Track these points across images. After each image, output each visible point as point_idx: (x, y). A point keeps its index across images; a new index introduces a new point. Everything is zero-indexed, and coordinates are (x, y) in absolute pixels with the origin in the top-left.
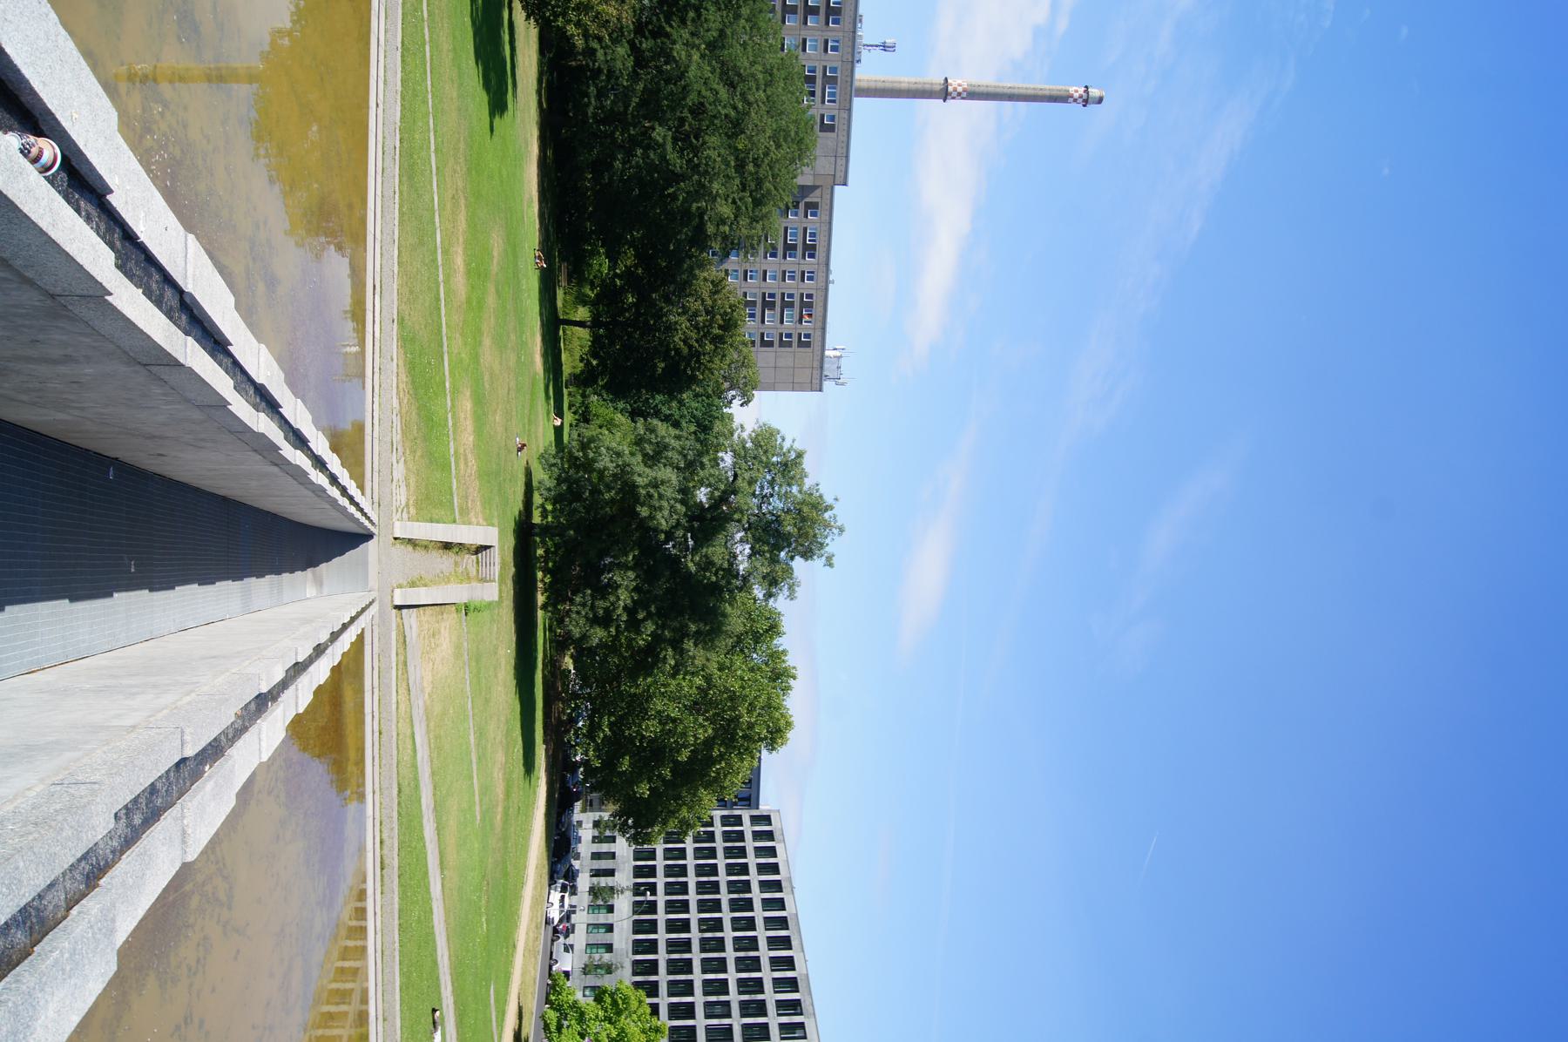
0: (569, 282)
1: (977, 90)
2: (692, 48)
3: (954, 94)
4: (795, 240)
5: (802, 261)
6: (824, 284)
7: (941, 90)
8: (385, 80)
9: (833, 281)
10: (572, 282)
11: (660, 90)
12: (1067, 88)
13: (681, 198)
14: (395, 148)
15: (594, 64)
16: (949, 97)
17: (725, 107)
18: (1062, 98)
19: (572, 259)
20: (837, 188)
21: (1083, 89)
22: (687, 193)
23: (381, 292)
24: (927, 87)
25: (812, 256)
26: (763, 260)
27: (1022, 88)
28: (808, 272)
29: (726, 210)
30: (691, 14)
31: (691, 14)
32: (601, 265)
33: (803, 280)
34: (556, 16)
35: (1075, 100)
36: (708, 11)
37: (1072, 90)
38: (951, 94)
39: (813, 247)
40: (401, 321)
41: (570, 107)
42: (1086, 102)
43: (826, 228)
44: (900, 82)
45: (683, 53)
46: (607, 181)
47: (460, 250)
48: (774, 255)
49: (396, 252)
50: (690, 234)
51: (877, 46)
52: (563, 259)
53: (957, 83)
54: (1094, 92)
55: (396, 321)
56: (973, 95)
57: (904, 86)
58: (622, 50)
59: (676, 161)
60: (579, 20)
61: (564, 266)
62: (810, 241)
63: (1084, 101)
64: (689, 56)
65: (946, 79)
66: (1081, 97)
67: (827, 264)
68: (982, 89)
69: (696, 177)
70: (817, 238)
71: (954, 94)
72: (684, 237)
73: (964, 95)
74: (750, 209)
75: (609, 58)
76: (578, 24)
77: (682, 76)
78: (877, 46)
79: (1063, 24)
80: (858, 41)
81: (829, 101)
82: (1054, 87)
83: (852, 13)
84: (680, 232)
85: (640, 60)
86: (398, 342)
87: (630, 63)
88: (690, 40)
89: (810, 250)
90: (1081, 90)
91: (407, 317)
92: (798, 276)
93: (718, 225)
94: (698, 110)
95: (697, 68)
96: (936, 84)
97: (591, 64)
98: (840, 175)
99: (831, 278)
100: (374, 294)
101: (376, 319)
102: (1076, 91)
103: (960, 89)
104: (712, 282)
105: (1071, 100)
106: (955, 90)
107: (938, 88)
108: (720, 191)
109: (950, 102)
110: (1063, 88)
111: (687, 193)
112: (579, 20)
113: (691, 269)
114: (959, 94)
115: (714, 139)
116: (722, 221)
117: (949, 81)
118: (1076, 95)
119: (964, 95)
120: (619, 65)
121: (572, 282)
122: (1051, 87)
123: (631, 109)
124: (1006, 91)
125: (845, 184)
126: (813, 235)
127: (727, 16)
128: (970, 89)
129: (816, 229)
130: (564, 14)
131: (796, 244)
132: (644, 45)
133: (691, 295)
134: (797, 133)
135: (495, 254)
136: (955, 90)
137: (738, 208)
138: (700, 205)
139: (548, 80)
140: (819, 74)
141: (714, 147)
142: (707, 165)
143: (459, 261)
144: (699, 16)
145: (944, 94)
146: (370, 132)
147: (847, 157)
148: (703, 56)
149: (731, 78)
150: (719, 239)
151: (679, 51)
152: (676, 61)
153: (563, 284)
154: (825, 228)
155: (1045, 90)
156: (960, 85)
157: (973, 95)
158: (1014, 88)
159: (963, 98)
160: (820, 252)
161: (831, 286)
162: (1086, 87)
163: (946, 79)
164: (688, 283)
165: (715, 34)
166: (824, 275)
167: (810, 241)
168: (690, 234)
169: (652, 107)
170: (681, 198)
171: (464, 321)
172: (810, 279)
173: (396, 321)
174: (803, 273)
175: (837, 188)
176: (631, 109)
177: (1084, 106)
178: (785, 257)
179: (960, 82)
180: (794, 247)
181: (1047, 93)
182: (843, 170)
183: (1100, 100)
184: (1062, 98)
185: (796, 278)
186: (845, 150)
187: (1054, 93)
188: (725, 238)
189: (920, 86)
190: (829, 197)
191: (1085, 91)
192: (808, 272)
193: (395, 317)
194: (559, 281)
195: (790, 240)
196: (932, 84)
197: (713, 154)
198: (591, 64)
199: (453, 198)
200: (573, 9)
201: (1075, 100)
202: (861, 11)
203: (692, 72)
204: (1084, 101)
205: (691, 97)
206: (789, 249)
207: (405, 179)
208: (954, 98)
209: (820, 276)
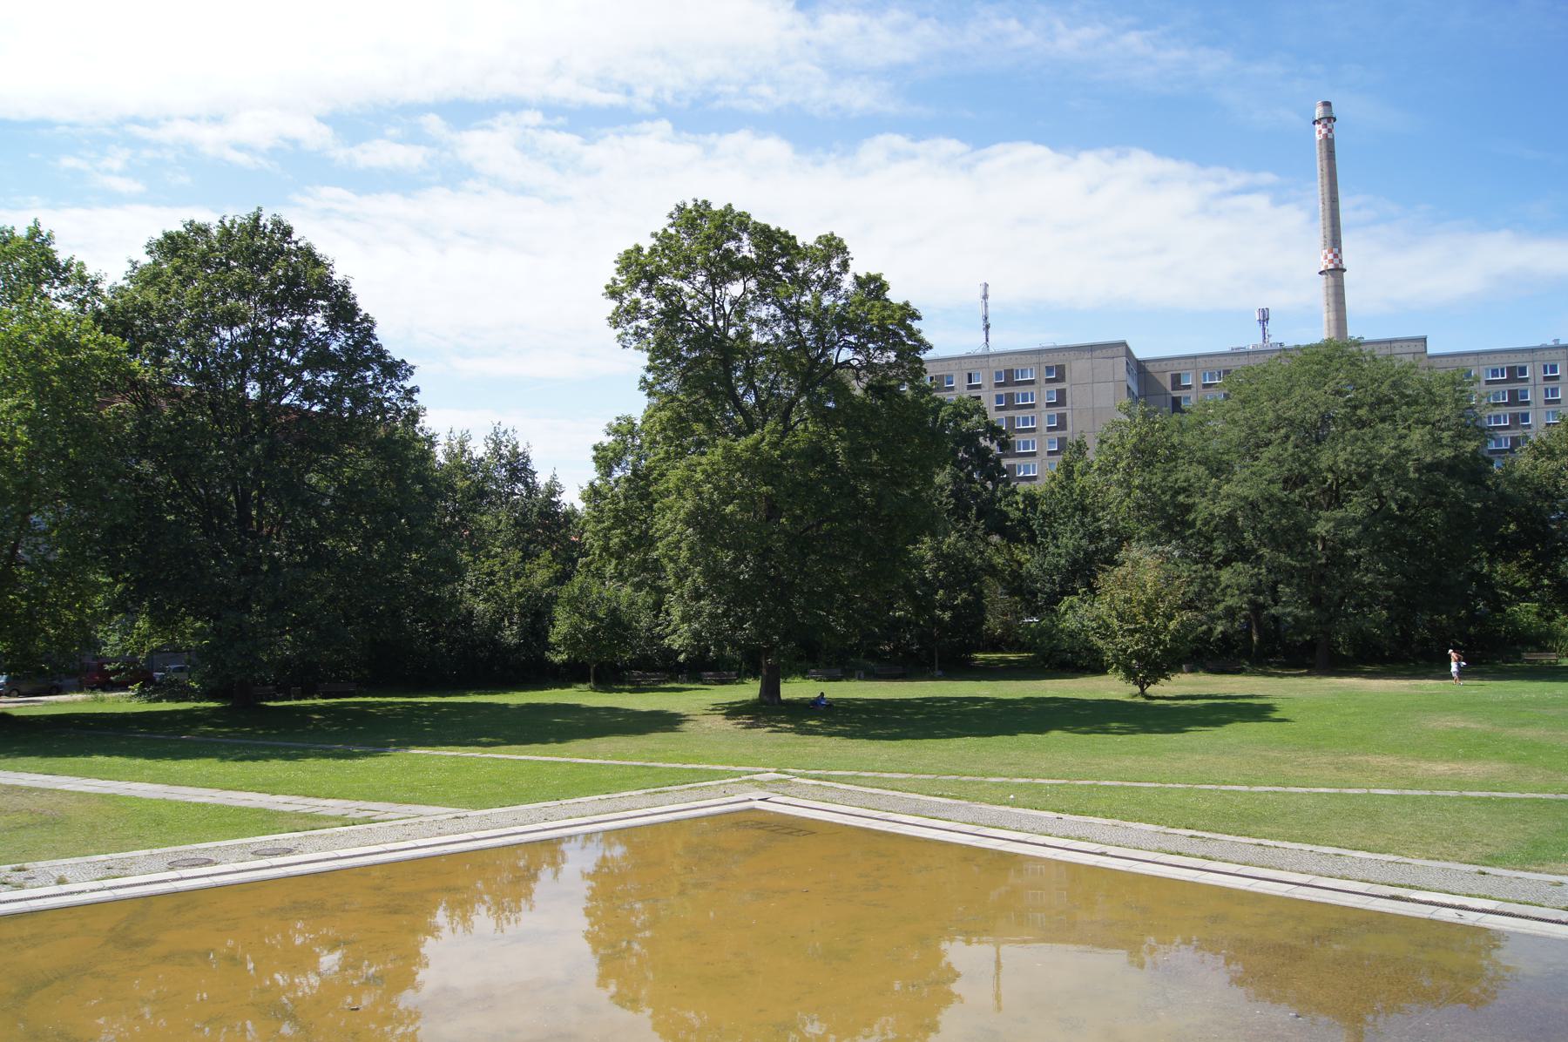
0: (1551, 650)
1: (1329, 238)
2: (1219, 494)
3: (1336, 261)
4: (1504, 392)
5: (1531, 382)
6: (1560, 351)
7: (1333, 276)
8: (1203, 857)
9: (1555, 340)
10: (1551, 647)
11: (1270, 529)
12: (1317, 143)
13: (1404, 494)
14: (1192, 837)
15: (1244, 609)
16: (1340, 266)
17: (1286, 450)
18: (1329, 145)
19: (1518, 647)
20: (1430, 351)
21: (1317, 126)
22: (1397, 485)
23: (1411, 887)
24: (1331, 291)
25: (1523, 370)
26: (1533, 429)
27: (1323, 190)
28: (1545, 372)
29: (1417, 437)
30: (1181, 498)
31: (1181, 498)
32: (1528, 612)
33: (1557, 378)
34: (1159, 642)
35: (1330, 131)
36: (1176, 480)
37: (1318, 137)
38: (1336, 265)
39: (1511, 370)
40: (1493, 860)
41: (1300, 639)
42: (1330, 119)
43: (1485, 358)
44: (1328, 321)
45: (1223, 503)
46: (1391, 592)
47: (1424, 765)
48: (1525, 417)
49: (1359, 854)
50: (1458, 484)
51: (1264, 329)
52: (1519, 658)
53: (1323, 261)
54: (1319, 112)
55: (1483, 869)
56: (1335, 242)
57: (1332, 316)
58: (1225, 575)
59: (1356, 508)
60: (1164, 615)
61: (1526, 656)
62: (1503, 376)
63: (1329, 122)
64: (1228, 497)
65: (1320, 273)
66: (1325, 126)
67: (1533, 350)
68: (1328, 234)
69: (1376, 477)
70: (1498, 367)
71: (1336, 261)
72: (1461, 490)
73: (1336, 250)
74: (1419, 408)
75: (1237, 592)
76: (1170, 617)
77: (1253, 505)
78: (1264, 329)
79: (1267, 177)
80: (1259, 348)
81: (1032, 400)
82: (1318, 157)
83: (1228, 358)
84: (1455, 495)
85: (1243, 553)
86: (1527, 870)
87: (1239, 566)
88: (1209, 497)
89: (1515, 373)
90: (1318, 127)
91: (1489, 850)
92: (1551, 385)
93: (1442, 446)
94: (1290, 482)
95: (1242, 486)
96: (1327, 283)
97: (1244, 613)
98: (1413, 347)
99: (1550, 343)
100: (1408, 900)
101: (1457, 903)
102: (1320, 132)
103: (1330, 256)
104: (1536, 458)
105: (1330, 136)
106: (1331, 261)
107: (1331, 280)
108: (1392, 445)
109: (1345, 264)
110: (1317, 146)
111: (1397, 485)
112: (1164, 615)
113: (1512, 483)
114: (1336, 256)
115: (1323, 458)
116: (1437, 442)
117: (1323, 269)
118: (1324, 131)
119: (1336, 250)
120: (1244, 580)
121: (1551, 647)
122: (1318, 159)
123: (1293, 563)
124: (1327, 207)
125: (1424, 340)
126: (1495, 373)
127: (1183, 458)
128: (1328, 246)
129: (1487, 369)
130: (1156, 632)
131: (1509, 391)
132: (1220, 551)
133: (1556, 485)
134: (1319, 363)
135: (1462, 725)
136: (1331, 261)
137: (1418, 422)
138: (1412, 469)
139: (1275, 668)
140: (1003, 391)
141: (1334, 457)
142: (1358, 464)
143: (1441, 768)
144: (1184, 490)
145: (1336, 272)
146: (1131, 870)
147: (1391, 341)
148: (1228, 481)
149: (1253, 446)
150: (1461, 443)
151: (1221, 509)
152: (1235, 510)
153: (1552, 657)
154: (1485, 359)
155: (1322, 165)
156: (1326, 258)
157: (1335, 242)
158: (1323, 199)
159: (1340, 251)
160: (1515, 361)
161: (1561, 343)
162: (1314, 123)
163: (1320, 273)
164: (1539, 492)
165: (1202, 468)
166: (1547, 352)
167: (1503, 376)
168: (1458, 484)
169: (1294, 538)
170: (1404, 494)
171: (1545, 767)
172: (1554, 369)
173: (1483, 869)
174: (1546, 379)
175: (1430, 351)
176: (1293, 563)
177: (1335, 120)
178: (1527, 403)
179: (1322, 258)
180: (1513, 394)
181: (1325, 162)
182: (1406, 344)
183: (1327, 104)
184: (1329, 145)
185: (1555, 386)
186: (1382, 346)
187: (1324, 155)
188: (1460, 436)
189: (1331, 299)
190: (1444, 360)
191: (1319, 123)
192: (1545, 372)
193: (1477, 868)
194: (1550, 663)
195: (1504, 399)
196: (1327, 287)
197: (1343, 456)
198: (1244, 613)
199: (1338, 769)
200: (1151, 621)
201: (1330, 131)
202: (1227, 349)
203: (1242, 491)
204: (1329, 122)
205: (1276, 491)
206: (1515, 398)
207: (1253, 828)
208: (1341, 261)
209: (1549, 358)
